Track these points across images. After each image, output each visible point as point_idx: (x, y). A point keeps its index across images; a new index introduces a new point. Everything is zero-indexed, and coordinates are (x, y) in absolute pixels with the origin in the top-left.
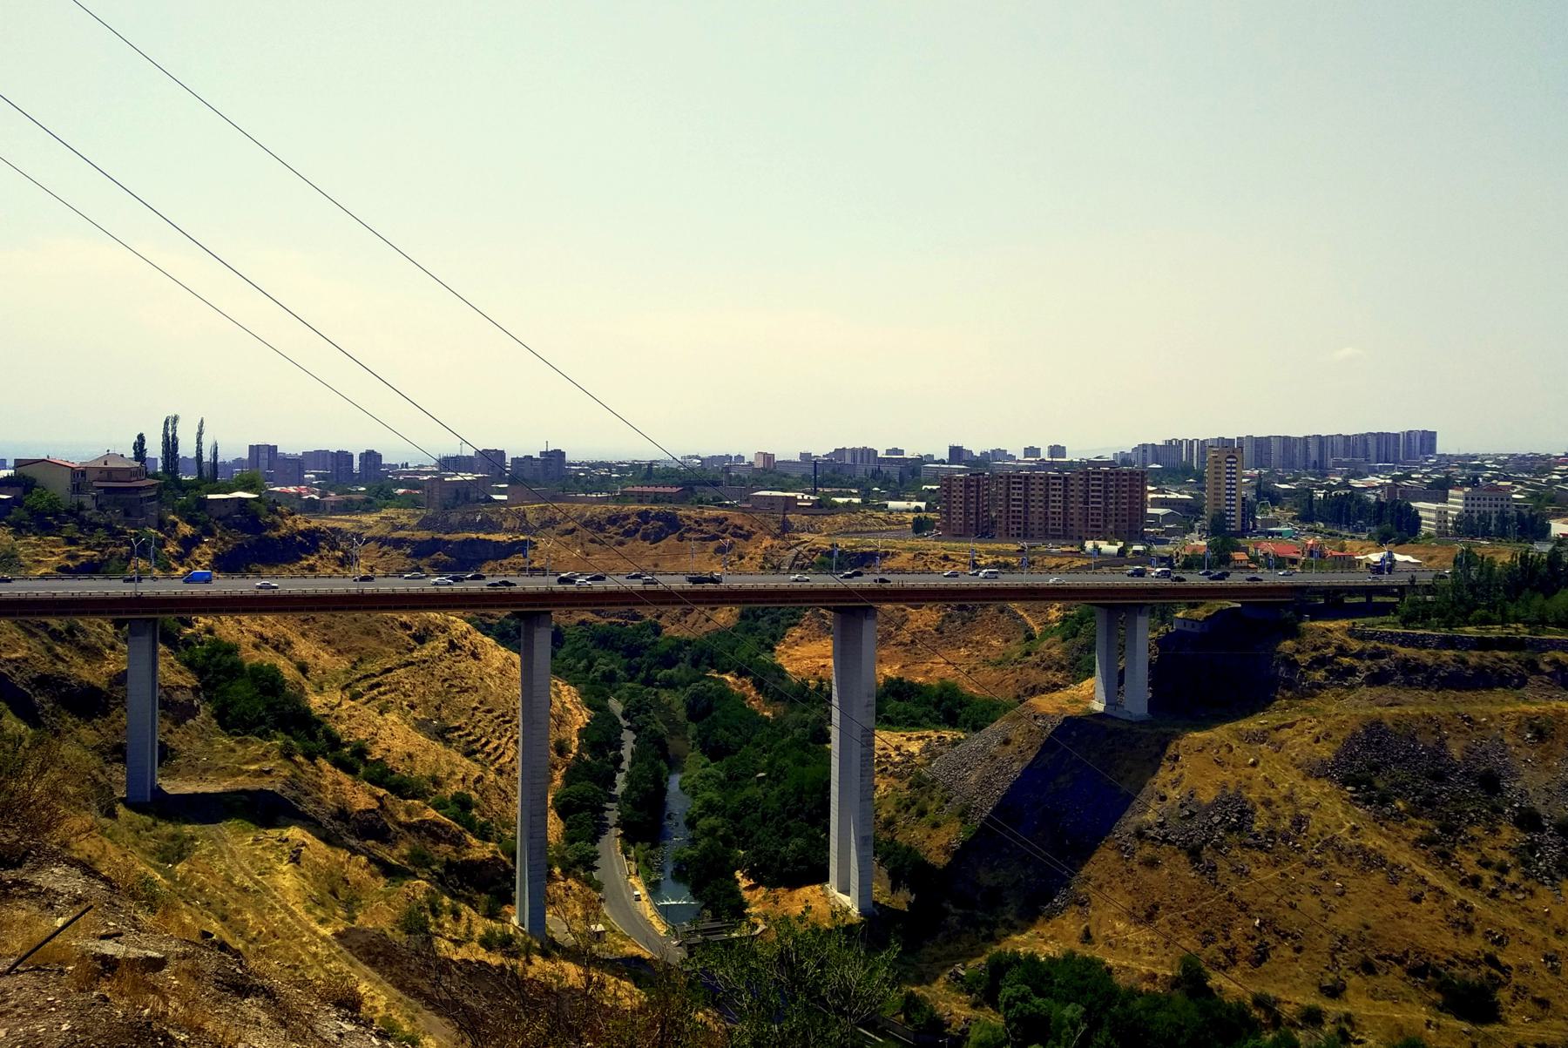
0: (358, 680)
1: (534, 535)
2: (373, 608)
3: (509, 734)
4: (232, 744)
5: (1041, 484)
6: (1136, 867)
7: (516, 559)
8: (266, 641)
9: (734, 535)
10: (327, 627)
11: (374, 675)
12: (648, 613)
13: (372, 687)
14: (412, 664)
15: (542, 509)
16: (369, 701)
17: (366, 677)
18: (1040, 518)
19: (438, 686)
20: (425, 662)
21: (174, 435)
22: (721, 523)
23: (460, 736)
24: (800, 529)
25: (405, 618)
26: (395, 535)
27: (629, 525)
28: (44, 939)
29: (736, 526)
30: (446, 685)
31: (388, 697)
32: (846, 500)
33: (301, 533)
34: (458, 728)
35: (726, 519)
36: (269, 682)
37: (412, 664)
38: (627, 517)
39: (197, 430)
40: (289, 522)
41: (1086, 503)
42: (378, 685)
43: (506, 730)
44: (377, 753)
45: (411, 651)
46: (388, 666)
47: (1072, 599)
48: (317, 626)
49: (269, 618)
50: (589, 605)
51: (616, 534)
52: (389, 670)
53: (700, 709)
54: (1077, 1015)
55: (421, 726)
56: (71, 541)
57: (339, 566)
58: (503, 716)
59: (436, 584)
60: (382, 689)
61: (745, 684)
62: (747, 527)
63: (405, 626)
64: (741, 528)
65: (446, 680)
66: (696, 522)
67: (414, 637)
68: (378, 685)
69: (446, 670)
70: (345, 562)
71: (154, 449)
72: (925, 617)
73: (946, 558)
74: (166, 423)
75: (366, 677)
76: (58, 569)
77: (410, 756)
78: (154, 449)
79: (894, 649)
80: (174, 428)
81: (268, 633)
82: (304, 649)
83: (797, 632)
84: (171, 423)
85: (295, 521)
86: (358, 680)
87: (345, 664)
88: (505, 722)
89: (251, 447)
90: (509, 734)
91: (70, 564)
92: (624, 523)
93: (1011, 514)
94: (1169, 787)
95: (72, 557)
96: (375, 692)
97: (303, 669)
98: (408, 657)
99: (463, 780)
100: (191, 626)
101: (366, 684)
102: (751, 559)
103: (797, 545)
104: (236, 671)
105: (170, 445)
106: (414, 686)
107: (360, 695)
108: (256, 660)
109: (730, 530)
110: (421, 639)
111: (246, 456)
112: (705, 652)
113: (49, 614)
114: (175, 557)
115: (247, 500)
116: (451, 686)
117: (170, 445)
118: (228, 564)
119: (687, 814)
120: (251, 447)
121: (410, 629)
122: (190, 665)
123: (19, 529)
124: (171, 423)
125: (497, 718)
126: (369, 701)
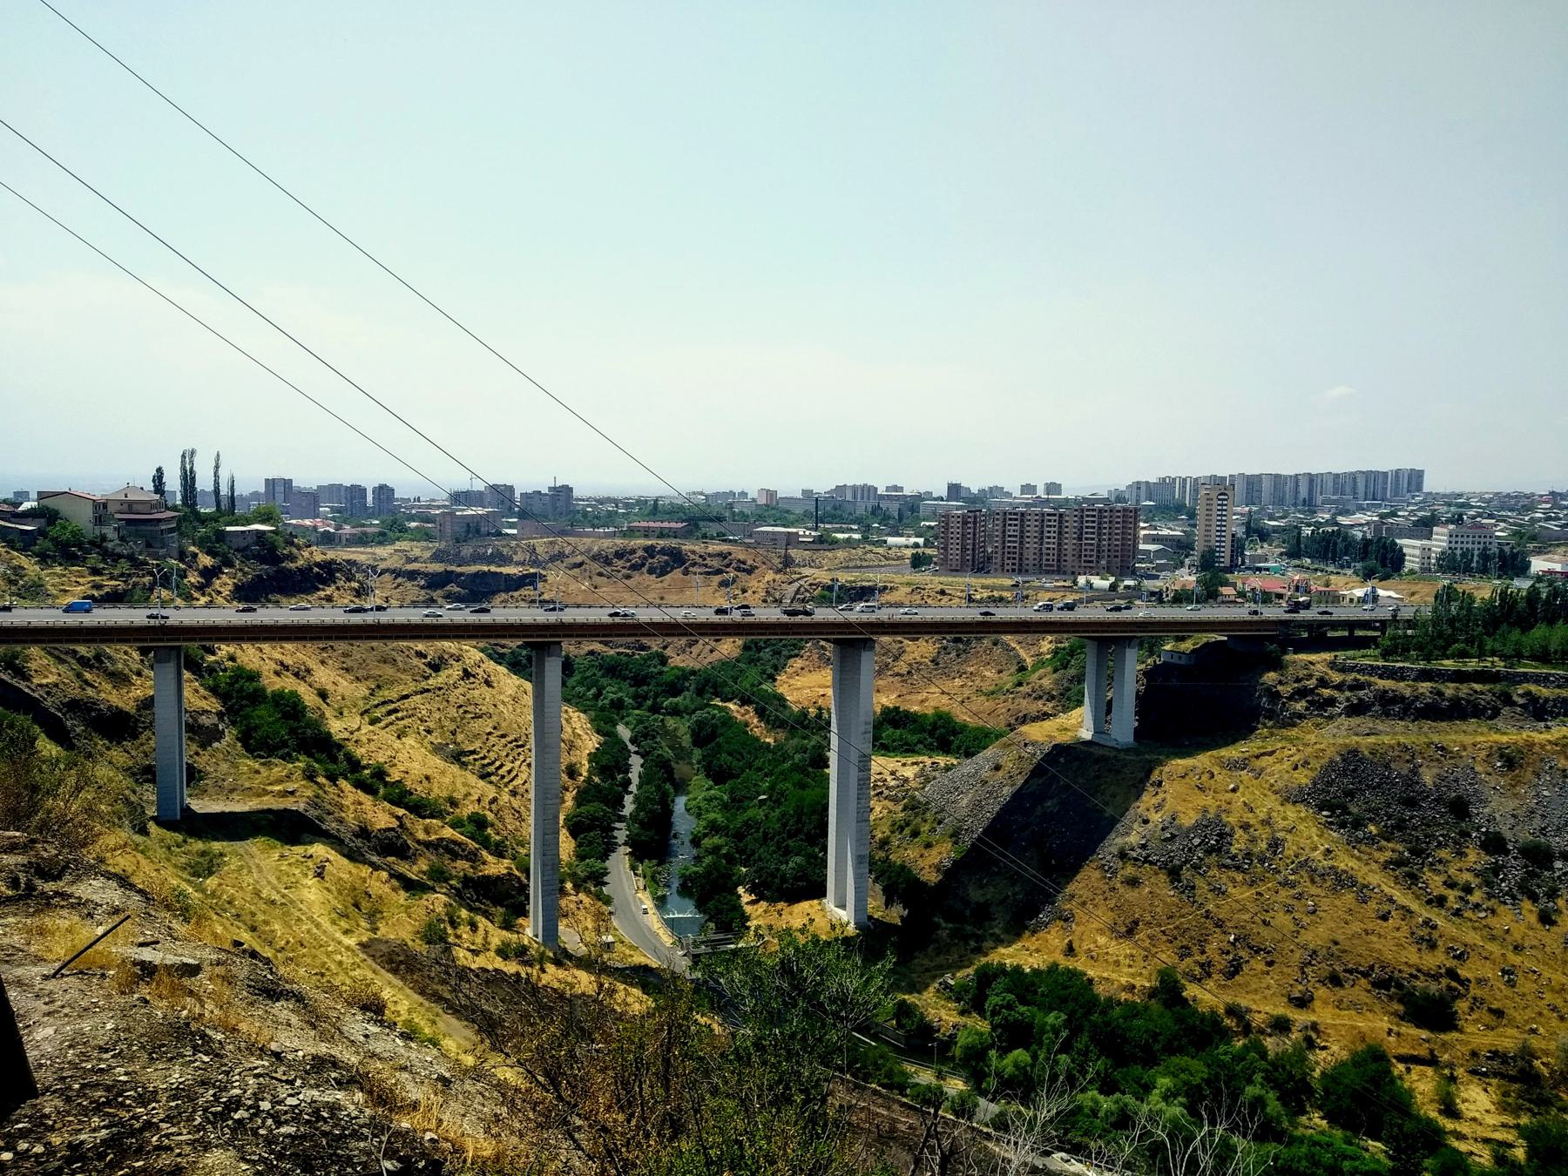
1: (544, 568)
3: (522, 758)
4: (257, 766)
6: (1118, 885)
7: (527, 591)
8: (287, 668)
9: (738, 569)
11: (392, 702)
12: (655, 644)
13: (390, 713)
15: (551, 543)
17: (384, 703)
19: (453, 712)
20: (440, 689)
21: (191, 469)
22: (725, 558)
23: (475, 760)
26: (410, 567)
27: (635, 559)
29: (739, 561)
30: (461, 711)
34: (473, 752)
36: (290, 707)
38: (633, 552)
39: (214, 464)
40: (306, 554)
41: (1080, 539)
43: (519, 754)
44: (395, 775)
45: (427, 678)
48: (335, 654)
50: (597, 636)
52: (406, 697)
53: (704, 735)
55: (437, 749)
56: (95, 572)
58: (516, 740)
60: (400, 715)
62: (750, 562)
63: (420, 655)
64: (744, 563)
65: (460, 706)
66: (701, 556)
67: (429, 665)
68: (396, 711)
72: (922, 649)
73: (943, 592)
74: (183, 456)
75: (384, 703)
77: (427, 778)
80: (192, 462)
81: (289, 661)
82: (324, 676)
83: (798, 663)
84: (188, 457)
88: (518, 747)
89: (267, 480)
90: (522, 758)
91: (96, 593)
95: (97, 587)
96: (393, 717)
98: (424, 685)
100: (214, 653)
101: (384, 709)
104: (258, 696)
105: (188, 479)
110: (436, 667)
111: (262, 490)
115: (264, 532)
116: (466, 712)
117: (188, 479)
120: (267, 480)
123: (44, 559)
124: (188, 457)
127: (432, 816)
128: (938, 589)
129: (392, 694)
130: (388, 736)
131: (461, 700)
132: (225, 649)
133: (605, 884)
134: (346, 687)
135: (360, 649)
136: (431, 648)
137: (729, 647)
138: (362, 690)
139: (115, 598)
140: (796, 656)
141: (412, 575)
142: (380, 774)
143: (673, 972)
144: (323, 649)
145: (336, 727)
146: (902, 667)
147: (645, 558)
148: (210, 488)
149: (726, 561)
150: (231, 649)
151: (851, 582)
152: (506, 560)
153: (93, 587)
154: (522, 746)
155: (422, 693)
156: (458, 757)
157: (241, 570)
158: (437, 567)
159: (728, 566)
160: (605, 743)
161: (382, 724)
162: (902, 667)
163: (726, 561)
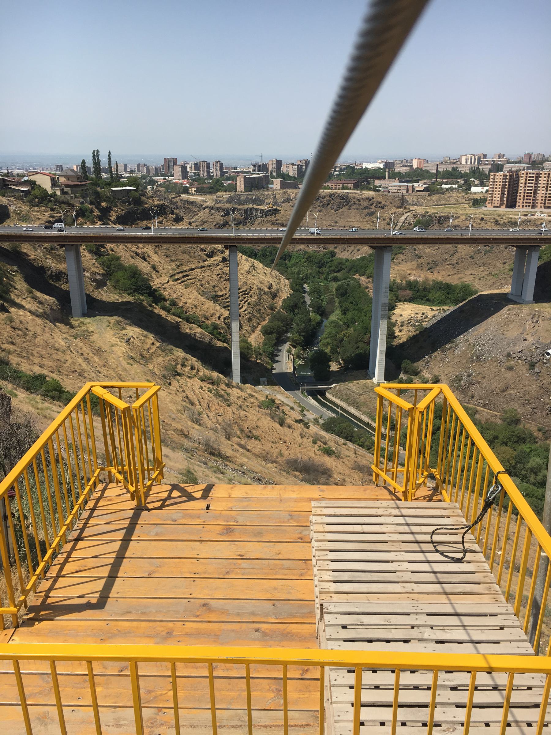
2: (209, 243)
3: (246, 299)
4: (118, 297)
5: (545, 177)
7: (272, 218)
8: (138, 254)
10: (166, 249)
11: (186, 271)
12: (331, 247)
13: (184, 277)
14: (204, 267)
15: (284, 193)
16: (182, 282)
17: (182, 272)
18: (542, 197)
20: (210, 266)
22: (370, 200)
23: (222, 299)
24: (412, 203)
25: (203, 246)
26: (217, 206)
29: (377, 202)
30: (219, 276)
32: (450, 186)
34: (222, 296)
35: (373, 198)
36: (135, 273)
37: (204, 267)
40: (151, 201)
42: (187, 276)
43: (245, 298)
45: (204, 261)
46: (193, 267)
48: (162, 248)
49: (141, 245)
50: (368, 243)
51: (318, 206)
52: (193, 269)
53: (343, 293)
55: (203, 294)
56: (52, 210)
57: (174, 222)
58: (245, 291)
59: (25, 230)
60: (189, 277)
61: (369, 282)
62: (383, 203)
63: (202, 250)
64: (380, 203)
66: (358, 200)
67: (206, 255)
68: (187, 276)
69: (220, 271)
70: (178, 219)
71: (90, 163)
72: (464, 250)
73: (482, 219)
74: (94, 153)
75: (182, 272)
77: (196, 306)
78: (90, 163)
80: (98, 156)
81: (139, 251)
82: (155, 258)
83: (402, 257)
84: (96, 154)
86: (178, 273)
87: (174, 265)
88: (245, 294)
90: (246, 299)
91: (51, 219)
92: (323, 200)
93: (526, 195)
94: (530, 335)
96: (186, 279)
99: (219, 318)
100: (105, 248)
101: (181, 275)
104: (121, 267)
105: (97, 163)
107: (178, 279)
108: (131, 263)
109: (375, 204)
110: (210, 256)
111: (163, 163)
113: (216, 243)
114: (96, 217)
115: (131, 190)
117: (97, 163)
118: (122, 220)
121: (205, 251)
122: (102, 264)
123: (32, 204)
124: (96, 154)
125: (241, 292)
126: (182, 282)
127: (193, 323)
128: (480, 218)
129: (185, 268)
132: (109, 246)
134: (166, 266)
136: (209, 247)
137: (366, 250)
138: (174, 265)
141: (218, 209)
142: (174, 304)
143: (67, 323)
144: (156, 246)
145: (156, 283)
146: (455, 259)
147: (330, 201)
148: (107, 166)
149: (371, 202)
150: (112, 246)
151: (435, 213)
152: (261, 202)
153: (50, 217)
154: (247, 294)
155: (201, 268)
157: (120, 209)
158: (228, 206)
159: (371, 205)
160: (293, 294)
161: (180, 281)
162: (455, 259)
163: (371, 202)
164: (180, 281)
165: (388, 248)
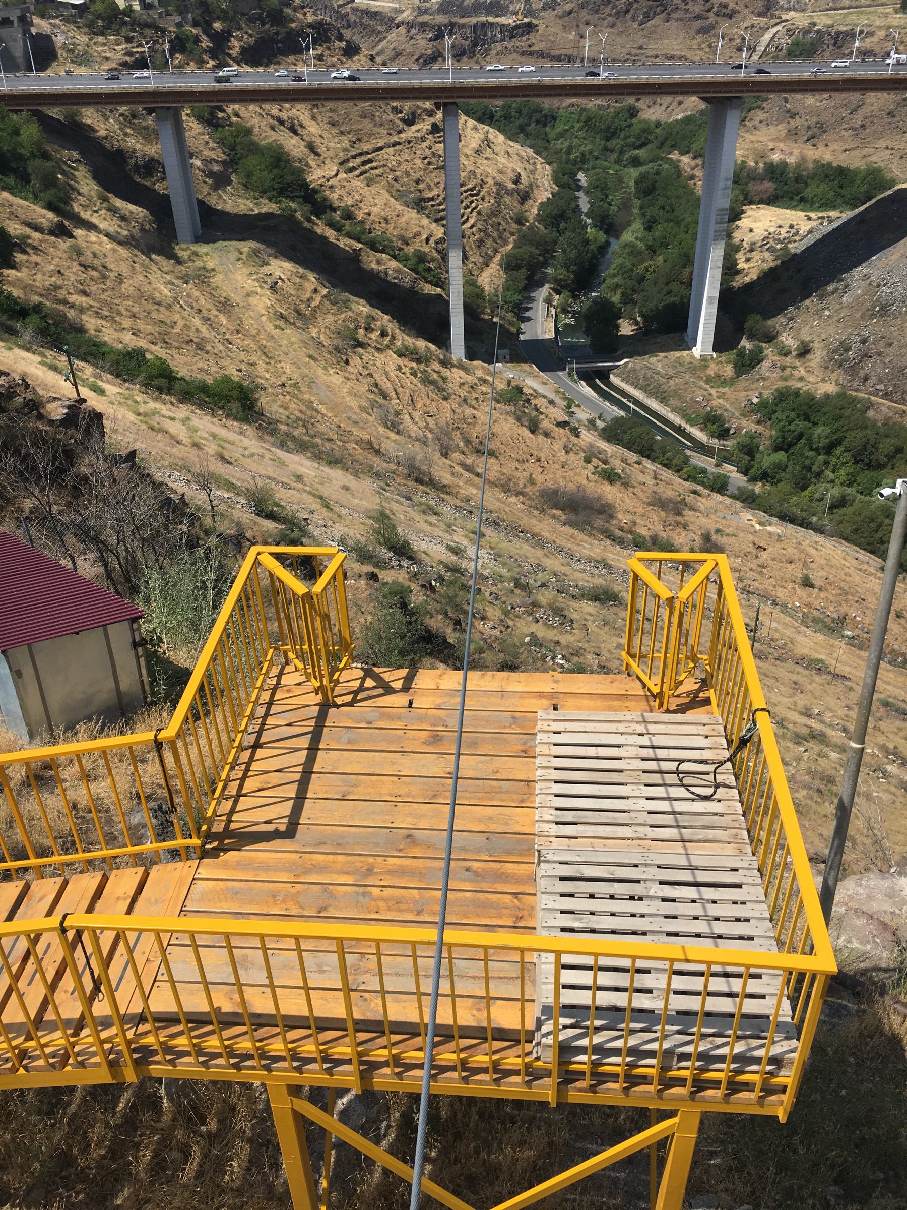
0: (354, 157)
1: (536, 18)
3: (473, 205)
7: (521, 43)
8: (282, 123)
11: (368, 153)
13: (364, 163)
14: (399, 143)
16: (361, 174)
17: (361, 154)
19: (418, 162)
20: (409, 142)
23: (433, 206)
26: (421, 19)
28: (884, 613)
31: (377, 172)
33: (310, 26)
34: (432, 199)
37: (399, 143)
42: (370, 161)
43: (472, 202)
44: (360, 215)
45: (400, 132)
47: (512, 96)
52: (380, 149)
54: (824, 434)
55: (399, 196)
56: (129, 40)
58: (472, 189)
60: (374, 164)
64: (726, 6)
65: (425, 158)
68: (370, 161)
75: (361, 154)
76: (120, 64)
77: (386, 220)
79: (844, 133)
81: (284, 116)
82: (313, 129)
83: (760, 115)
85: (305, 14)
86: (354, 157)
87: (346, 143)
88: (472, 195)
90: (473, 205)
95: (129, 54)
96: (367, 167)
97: (312, 147)
98: (395, 138)
99: (427, 240)
101: (359, 160)
102: (731, 40)
103: (777, 24)
104: (254, 148)
106: (399, 163)
107: (353, 169)
108: (270, 140)
109: (715, 9)
110: (410, 122)
112: (671, 134)
116: (429, 164)
119: (798, 308)
121: (401, 112)
122: (221, 142)
123: (94, 31)
126: (361, 174)
127: (383, 251)
129: (366, 147)
130: (358, 183)
131: (428, 152)
133: (528, 319)
135: (343, 107)
139: (141, 64)
140: (759, 107)
142: (348, 215)
145: (316, 176)
153: (125, 55)
155: (394, 145)
156: (420, 204)
160: (558, 193)
161: (357, 173)
164: (357, 173)
165: (735, 101)
